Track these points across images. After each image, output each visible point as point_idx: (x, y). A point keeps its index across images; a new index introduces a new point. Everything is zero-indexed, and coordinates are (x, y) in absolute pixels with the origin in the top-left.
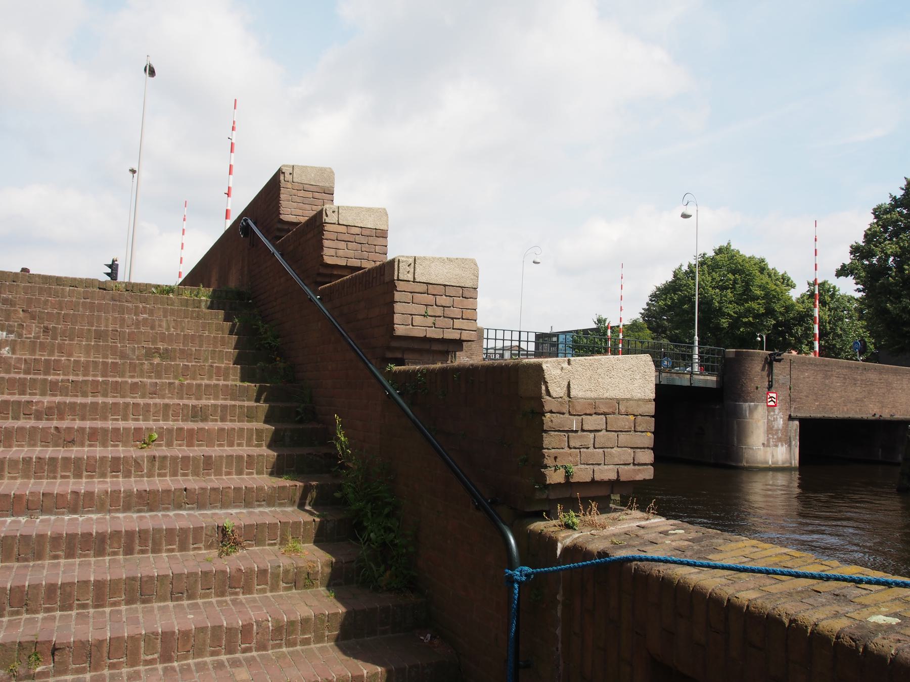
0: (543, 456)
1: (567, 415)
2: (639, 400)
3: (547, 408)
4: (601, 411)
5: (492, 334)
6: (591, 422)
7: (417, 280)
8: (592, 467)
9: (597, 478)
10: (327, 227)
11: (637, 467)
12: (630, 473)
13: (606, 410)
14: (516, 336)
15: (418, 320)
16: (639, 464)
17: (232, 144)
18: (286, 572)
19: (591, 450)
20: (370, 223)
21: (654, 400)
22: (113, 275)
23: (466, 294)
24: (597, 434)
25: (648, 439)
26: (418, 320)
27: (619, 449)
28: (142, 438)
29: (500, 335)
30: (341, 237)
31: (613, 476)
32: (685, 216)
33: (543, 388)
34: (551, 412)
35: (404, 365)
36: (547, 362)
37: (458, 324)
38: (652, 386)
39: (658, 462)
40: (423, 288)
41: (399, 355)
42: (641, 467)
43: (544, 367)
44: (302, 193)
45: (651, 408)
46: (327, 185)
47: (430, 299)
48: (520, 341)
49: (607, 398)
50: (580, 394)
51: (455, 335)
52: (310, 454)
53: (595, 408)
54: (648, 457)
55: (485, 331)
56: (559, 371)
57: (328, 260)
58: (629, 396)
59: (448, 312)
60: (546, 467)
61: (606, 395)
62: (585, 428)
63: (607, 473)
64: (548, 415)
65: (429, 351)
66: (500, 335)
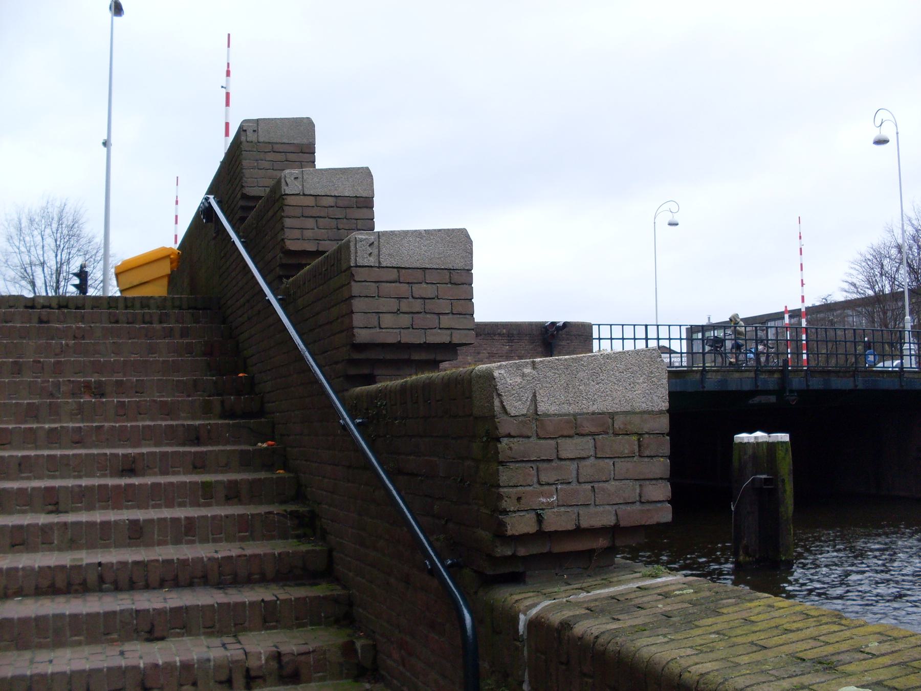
0: (500, 497)
1: (533, 439)
2: (643, 412)
3: (503, 430)
4: (586, 430)
5: (605, 332)
6: (570, 447)
7: (384, 264)
8: (576, 509)
9: (584, 524)
10: (290, 201)
11: (647, 507)
12: (634, 515)
13: (593, 430)
14: (640, 333)
15: (387, 320)
16: (648, 502)
17: (228, 95)
18: (218, 667)
19: (574, 485)
20: (348, 191)
21: (668, 411)
22: (82, 287)
23: (456, 278)
24: (583, 463)
25: (661, 466)
26: (387, 320)
27: (617, 483)
28: (52, 501)
29: (617, 333)
30: (308, 212)
31: (609, 520)
32: (881, 142)
33: (497, 403)
34: (509, 436)
35: (375, 383)
36: (499, 367)
37: (446, 321)
38: (664, 392)
39: (675, 501)
40: (393, 275)
41: (366, 371)
42: (651, 507)
43: (496, 374)
44: (271, 156)
45: (664, 423)
46: (305, 141)
47: (404, 289)
48: (647, 339)
49: (593, 413)
50: (553, 409)
51: (442, 338)
52: (270, 513)
53: (574, 426)
54: (662, 491)
55: (595, 329)
56: (519, 380)
57: (292, 246)
58: (629, 408)
59: (430, 305)
60: (505, 512)
61: (594, 408)
62: (563, 455)
63: (603, 517)
64: (505, 441)
65: (409, 363)
66: (617, 333)
